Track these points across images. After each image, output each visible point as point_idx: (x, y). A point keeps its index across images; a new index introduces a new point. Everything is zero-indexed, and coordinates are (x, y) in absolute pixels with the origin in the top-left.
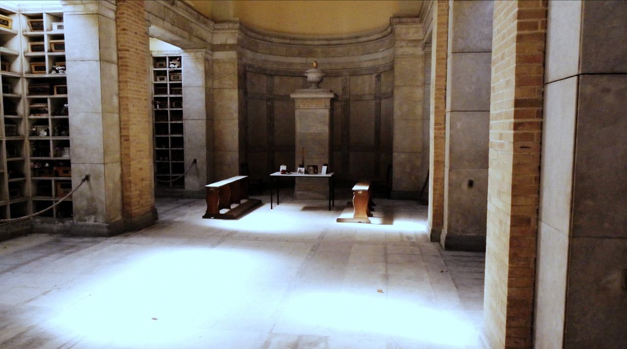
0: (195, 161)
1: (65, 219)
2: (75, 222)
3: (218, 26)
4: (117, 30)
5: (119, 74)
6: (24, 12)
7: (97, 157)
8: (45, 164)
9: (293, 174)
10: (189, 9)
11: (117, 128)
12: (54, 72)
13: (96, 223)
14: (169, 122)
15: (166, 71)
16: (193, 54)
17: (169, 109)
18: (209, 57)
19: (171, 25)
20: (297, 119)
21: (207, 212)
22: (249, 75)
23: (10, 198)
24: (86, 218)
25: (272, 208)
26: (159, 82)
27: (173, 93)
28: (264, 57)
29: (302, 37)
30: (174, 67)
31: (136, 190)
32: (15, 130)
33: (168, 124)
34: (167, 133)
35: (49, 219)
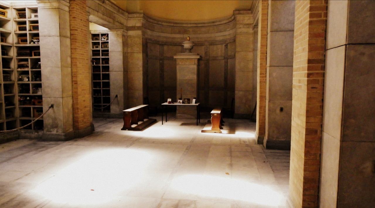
0: (117, 96)
2: (45, 132)
3: (130, 16)
4: (70, 18)
5: (71, 44)
6: (14, 7)
7: (58, 94)
9: (175, 104)
10: (113, 6)
11: (70, 77)
14: (101, 73)
16: (115, 32)
17: (101, 65)
18: (125, 34)
20: (178, 71)
22: (149, 45)
24: (52, 130)
25: (162, 124)
28: (158, 34)
30: (104, 40)
31: (81, 113)
32: (9, 77)
33: (100, 74)
35: (30, 130)
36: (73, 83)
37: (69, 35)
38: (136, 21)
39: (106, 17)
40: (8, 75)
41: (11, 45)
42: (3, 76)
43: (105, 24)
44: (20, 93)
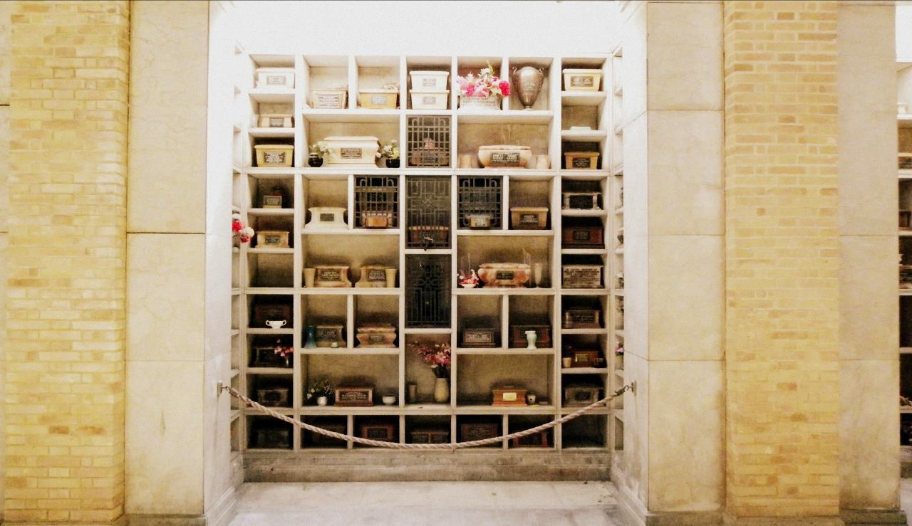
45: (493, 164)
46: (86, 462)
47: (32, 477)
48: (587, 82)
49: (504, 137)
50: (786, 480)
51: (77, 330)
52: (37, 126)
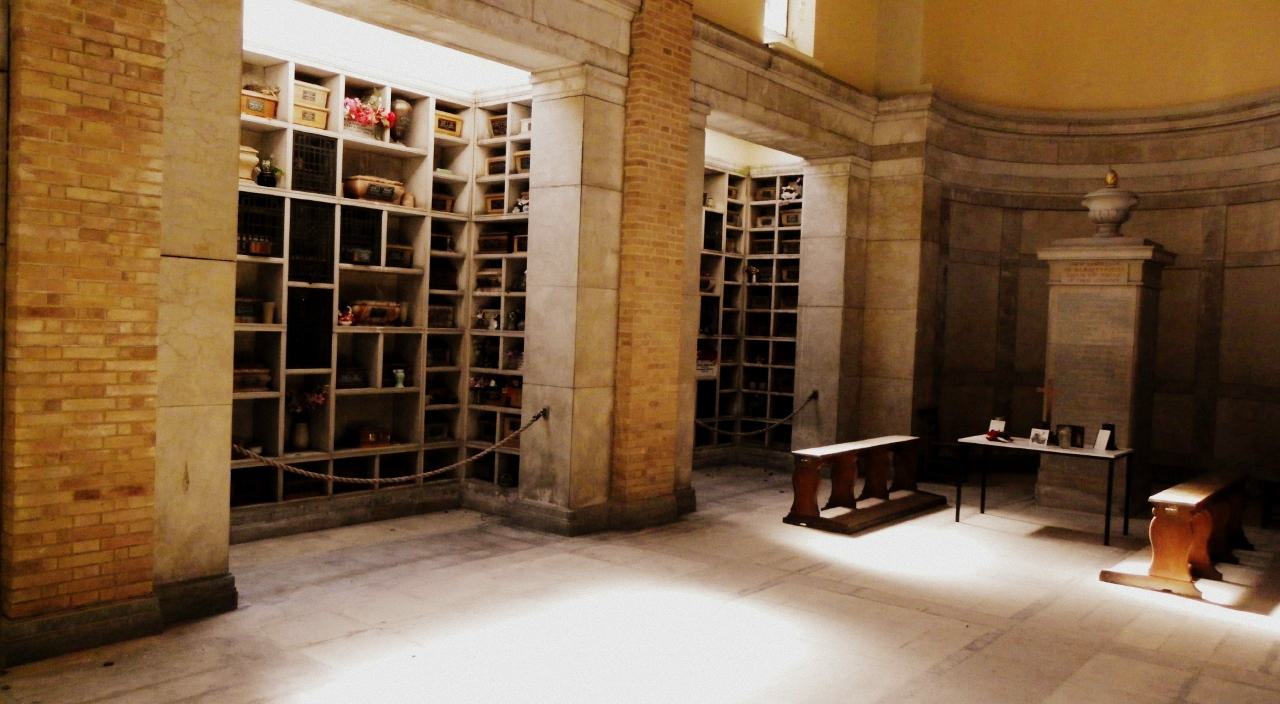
0: (815, 396)
1: (510, 490)
2: (520, 497)
3: (885, 106)
4: (626, 125)
5: (623, 212)
6: (481, 105)
7: (564, 375)
8: (490, 382)
9: (1019, 444)
10: (811, 75)
11: (610, 317)
12: (516, 210)
13: (554, 505)
14: (773, 311)
15: (773, 206)
16: (826, 168)
17: (773, 284)
18: (862, 173)
19: (762, 109)
20: (1053, 309)
21: (793, 508)
22: (955, 209)
23: (426, 437)
24: (538, 492)
25: (957, 520)
26: (761, 228)
27: (785, 250)
28: (1002, 168)
29: (1102, 116)
30: (789, 197)
31: (638, 447)
32: (451, 316)
33: (769, 314)
34: (767, 334)
35: (486, 485)
36: (620, 343)
37: (617, 181)
38: (906, 127)
39: (780, 116)
40: (445, 307)
41: (464, 219)
42: (430, 312)
43: (784, 142)
44: (477, 364)
45: (370, 194)
46: (121, 529)
47: (48, 557)
48: (451, 126)
49: (362, 165)
50: (650, 472)
51: (113, 371)
52: (61, 110)
